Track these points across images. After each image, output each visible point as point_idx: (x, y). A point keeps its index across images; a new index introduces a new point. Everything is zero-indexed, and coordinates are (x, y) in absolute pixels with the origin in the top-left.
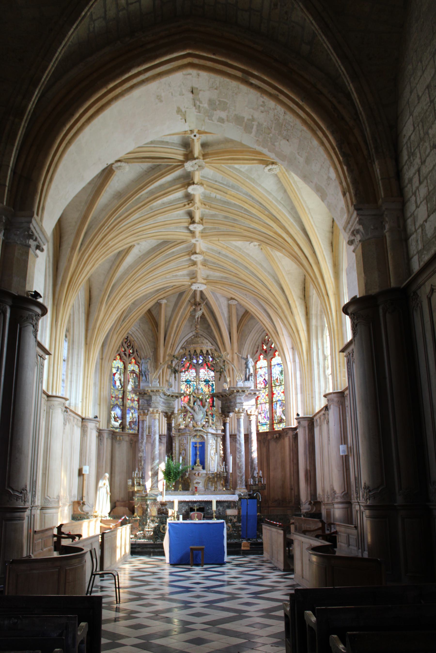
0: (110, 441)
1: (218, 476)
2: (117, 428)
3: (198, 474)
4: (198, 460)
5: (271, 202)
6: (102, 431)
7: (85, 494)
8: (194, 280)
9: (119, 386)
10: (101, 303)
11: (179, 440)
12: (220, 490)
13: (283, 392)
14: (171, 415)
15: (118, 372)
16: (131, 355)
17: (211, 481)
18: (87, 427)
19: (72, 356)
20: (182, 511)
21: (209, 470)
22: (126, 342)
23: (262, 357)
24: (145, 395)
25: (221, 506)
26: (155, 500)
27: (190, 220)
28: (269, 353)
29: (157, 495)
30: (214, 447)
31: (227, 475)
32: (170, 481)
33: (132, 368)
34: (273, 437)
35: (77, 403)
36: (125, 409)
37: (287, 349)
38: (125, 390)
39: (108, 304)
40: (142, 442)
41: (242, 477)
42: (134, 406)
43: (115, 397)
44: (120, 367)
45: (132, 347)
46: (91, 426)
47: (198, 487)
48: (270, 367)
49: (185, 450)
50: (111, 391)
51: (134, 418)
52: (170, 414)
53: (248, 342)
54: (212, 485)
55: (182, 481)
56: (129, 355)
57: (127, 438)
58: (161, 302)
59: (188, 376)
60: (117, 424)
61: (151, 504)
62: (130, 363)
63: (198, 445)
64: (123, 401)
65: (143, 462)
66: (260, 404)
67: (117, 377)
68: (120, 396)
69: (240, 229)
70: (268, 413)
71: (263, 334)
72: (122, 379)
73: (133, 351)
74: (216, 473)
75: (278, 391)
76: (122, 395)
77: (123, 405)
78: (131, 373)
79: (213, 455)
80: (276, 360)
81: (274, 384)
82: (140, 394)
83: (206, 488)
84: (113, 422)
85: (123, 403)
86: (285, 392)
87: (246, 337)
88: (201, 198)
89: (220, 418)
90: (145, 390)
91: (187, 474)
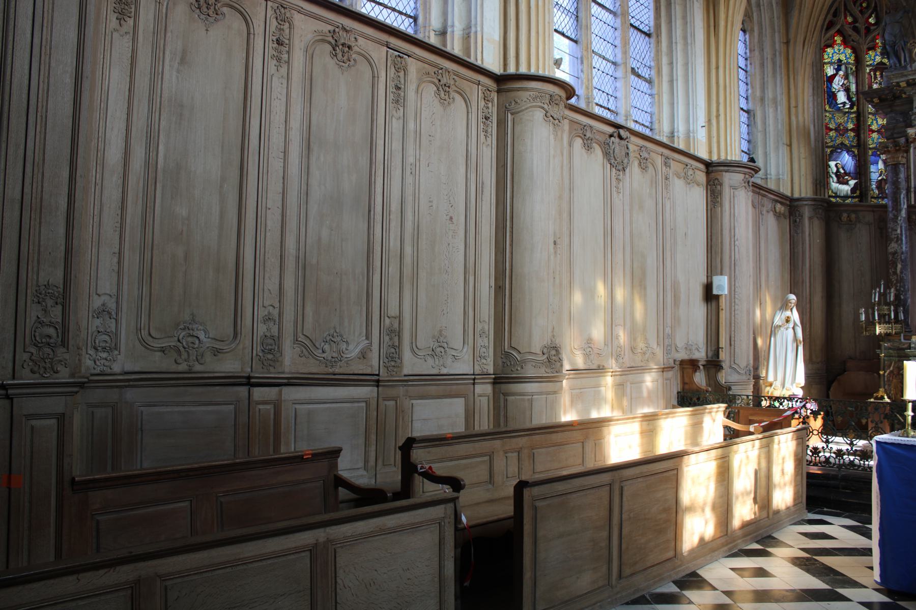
2: (846, 197)
6: (796, 203)
7: (723, 342)
9: (844, 104)
15: (841, 73)
16: (872, 28)
18: (721, 185)
19: (670, 22)
24: (898, 102)
40: (896, 217)
43: (836, 130)
56: (868, 30)
57: (869, 217)
60: (845, 189)
62: (869, 49)
64: (858, 135)
65: (899, 266)
72: (853, 88)
77: (859, 145)
78: (875, 71)
85: (859, 140)
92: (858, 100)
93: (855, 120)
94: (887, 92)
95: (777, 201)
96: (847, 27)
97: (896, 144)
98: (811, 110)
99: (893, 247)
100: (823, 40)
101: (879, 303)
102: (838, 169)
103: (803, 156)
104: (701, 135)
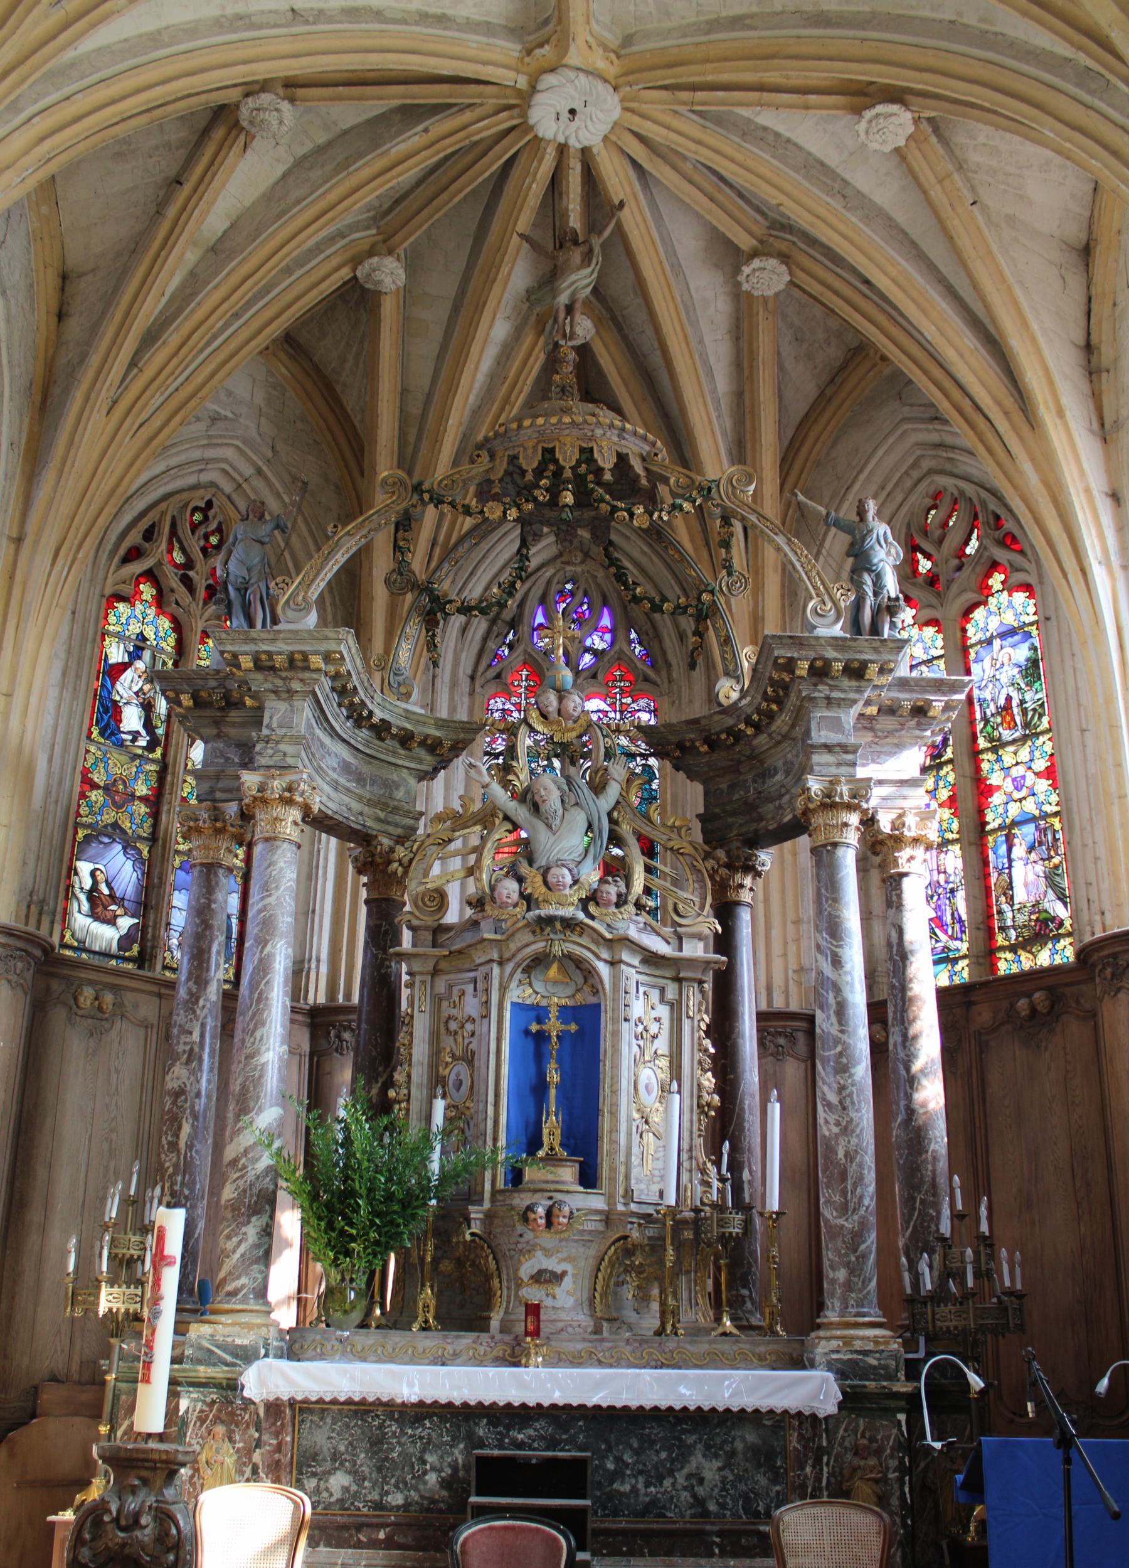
1: (688, 1234)
2: (106, 955)
3: (549, 1214)
4: (552, 1128)
9: (136, 735)
11: (437, 1000)
12: (696, 1332)
13: (1049, 773)
15: (140, 665)
17: (640, 1270)
20: (421, 1478)
21: (629, 1194)
24: (234, 715)
25: (710, 1451)
26: (233, 1386)
28: (950, 582)
29: (247, 1356)
30: (662, 1045)
31: (748, 1224)
32: (348, 1253)
36: (164, 859)
37: (1088, 491)
40: (194, 998)
41: (857, 1236)
43: (106, 789)
47: (548, 1302)
49: (469, 1058)
54: (643, 1298)
55: (446, 1266)
60: (106, 935)
61: (202, 1420)
63: (554, 1026)
64: (155, 815)
65: (186, 1129)
67: (128, 685)
70: (961, 895)
71: (913, 498)
74: (672, 1211)
76: (154, 782)
77: (153, 838)
79: (650, 1099)
80: (1006, 608)
81: (991, 740)
82: (199, 703)
83: (605, 1315)
85: (155, 826)
89: (700, 865)
91: (476, 1213)
92: (167, 735)
93: (154, 779)
94: (212, 683)
96: (169, 570)
97: (217, 816)
98: (49, 720)
99: (178, 1074)
100: (110, 581)
101: (119, 1225)
102: (95, 883)
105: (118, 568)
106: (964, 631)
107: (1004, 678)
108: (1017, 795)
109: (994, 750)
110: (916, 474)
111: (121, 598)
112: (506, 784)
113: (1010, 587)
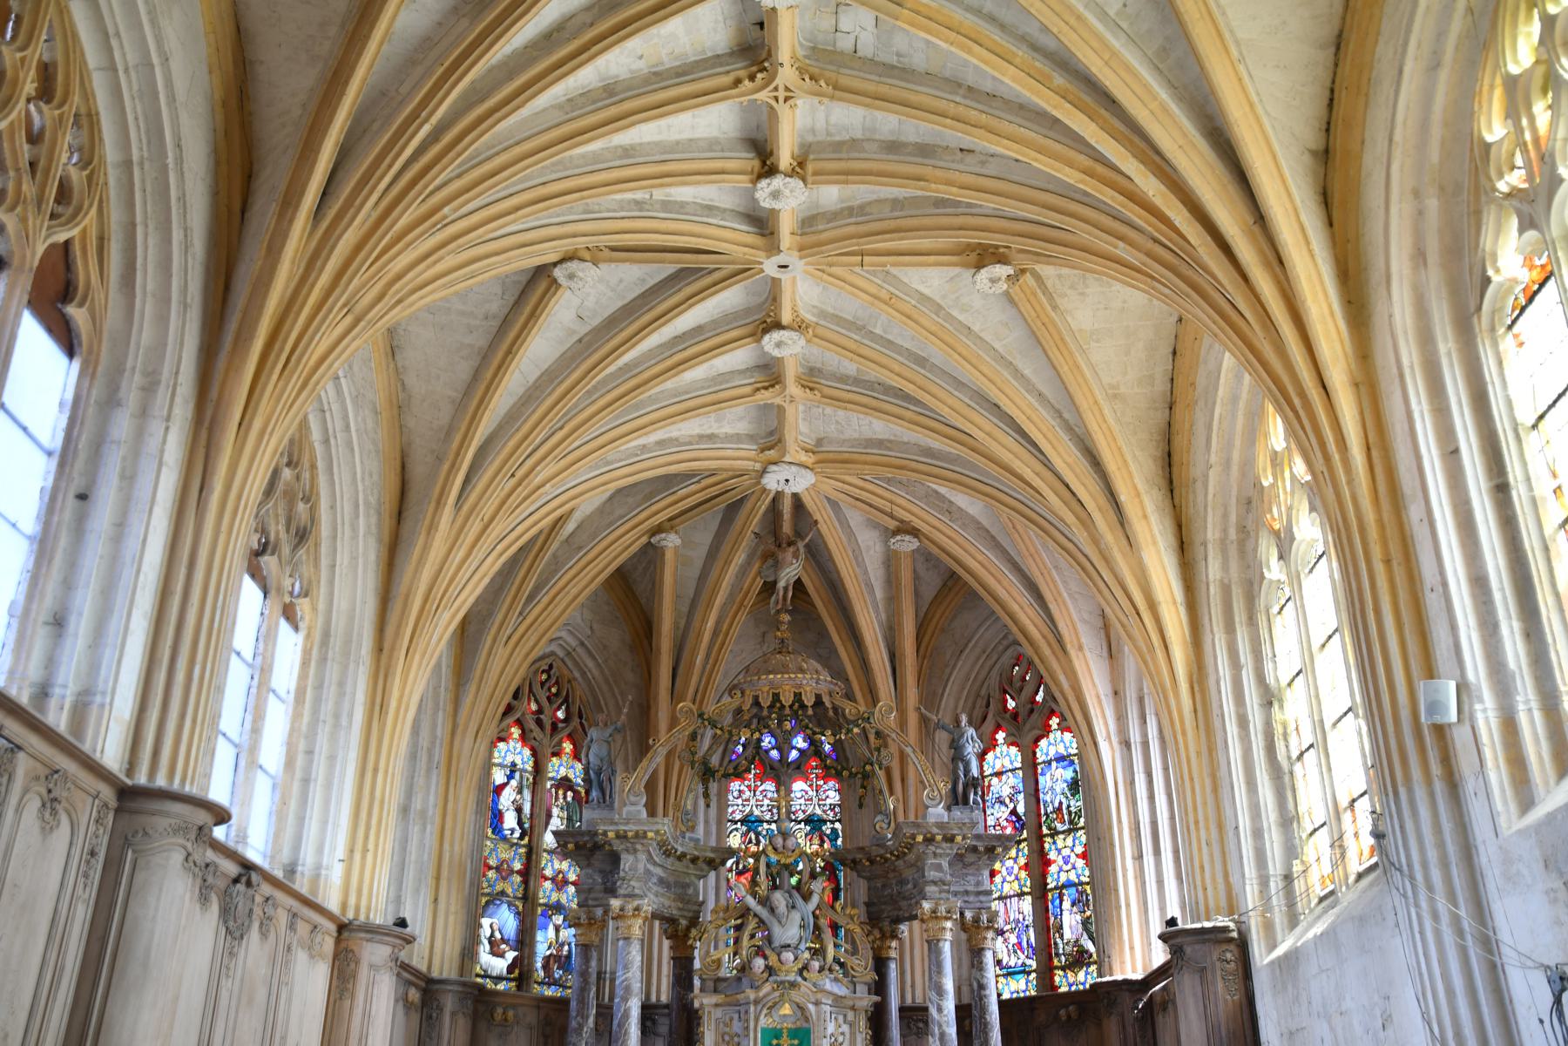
0: (463, 1024)
2: (499, 979)
5: (1079, 18)
8: (772, 454)
9: (513, 831)
10: (440, 503)
13: (1084, 856)
14: (688, 929)
15: (514, 783)
18: (357, 963)
22: (543, 684)
23: (1001, 736)
27: (756, 163)
33: (563, 772)
34: (1057, 1017)
35: (325, 862)
38: (534, 844)
39: (466, 508)
40: (581, 1027)
42: (564, 901)
43: (498, 869)
44: (520, 766)
45: (566, 700)
46: (375, 954)
48: (1031, 768)
50: (481, 847)
51: (562, 945)
52: (684, 922)
53: (957, 676)
56: (554, 727)
57: (531, 1017)
58: (664, 543)
59: (753, 802)
60: (499, 965)
62: (554, 754)
64: (526, 882)
66: (1000, 898)
67: (507, 798)
68: (517, 866)
69: (949, 183)
72: (527, 809)
73: (567, 711)
75: (1066, 852)
77: (525, 898)
78: (557, 787)
80: (1056, 743)
81: (1049, 828)
84: (485, 958)
85: (526, 889)
86: (1093, 856)
87: (947, 671)
88: (800, 53)
90: (596, 834)
95: (410, 983)
103: (453, 909)
104: (336, 874)
105: (304, 425)
106: (1034, 753)
107: (1058, 790)
108: (1065, 868)
109: (1052, 836)
110: (1005, 643)
111: (501, 739)
112: (754, 895)
113: (1064, 728)
